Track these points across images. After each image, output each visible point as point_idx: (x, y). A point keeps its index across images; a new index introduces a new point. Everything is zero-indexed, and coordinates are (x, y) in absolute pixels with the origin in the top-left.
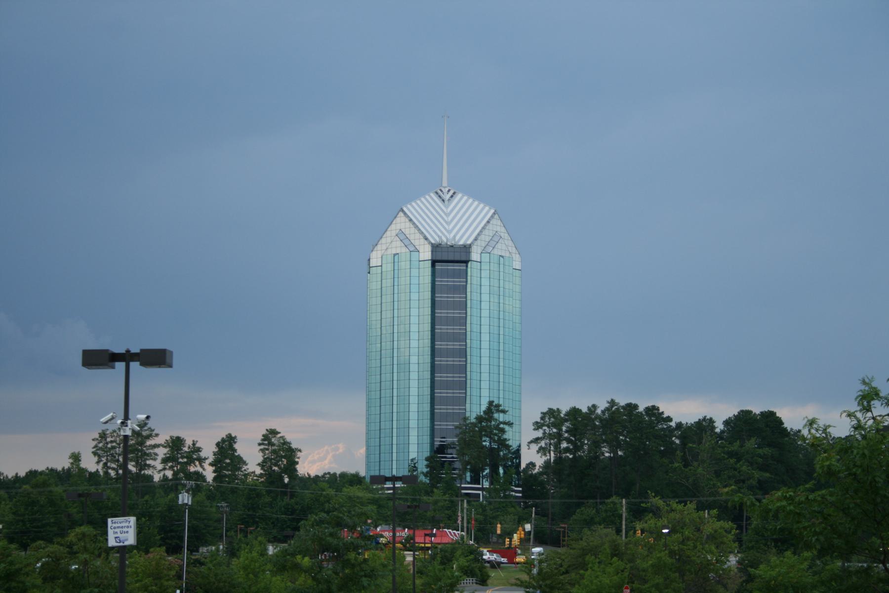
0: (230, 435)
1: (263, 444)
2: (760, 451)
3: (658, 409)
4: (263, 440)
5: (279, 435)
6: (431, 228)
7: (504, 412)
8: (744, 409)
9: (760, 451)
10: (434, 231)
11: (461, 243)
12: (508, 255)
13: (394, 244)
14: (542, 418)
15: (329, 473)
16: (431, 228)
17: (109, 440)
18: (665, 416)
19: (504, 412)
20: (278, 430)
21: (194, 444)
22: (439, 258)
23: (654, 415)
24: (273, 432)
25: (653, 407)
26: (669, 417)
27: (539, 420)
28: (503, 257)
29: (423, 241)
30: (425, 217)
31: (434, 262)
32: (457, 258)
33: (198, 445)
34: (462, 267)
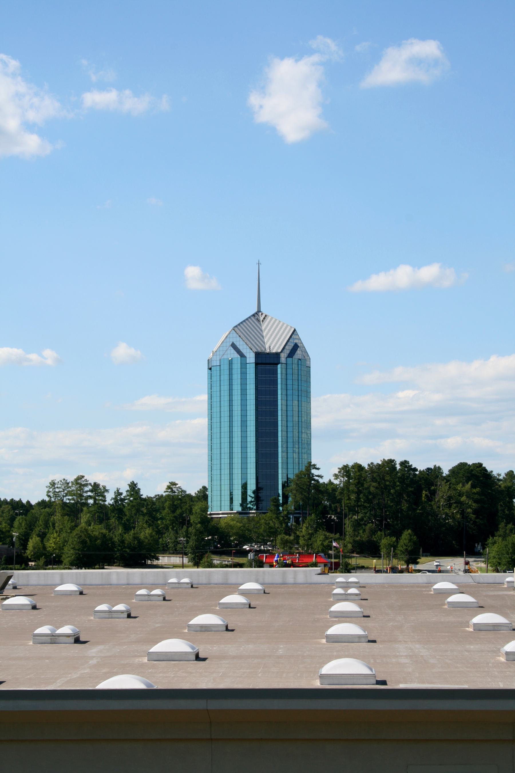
0: (133, 482)
1: (167, 492)
2: (474, 491)
3: (408, 462)
4: (167, 489)
5: (177, 486)
6: (254, 341)
7: (318, 469)
8: (462, 462)
9: (474, 491)
10: (255, 343)
11: (274, 351)
12: (303, 358)
13: (229, 352)
14: (339, 472)
15: (159, 495)
16: (254, 341)
17: (56, 486)
18: (413, 467)
19: (318, 469)
20: (177, 482)
21: (118, 491)
22: (260, 362)
23: (406, 467)
24: (174, 484)
25: (406, 461)
26: (415, 468)
27: (337, 473)
28: (300, 359)
29: (249, 350)
30: (278, 336)
31: (257, 364)
32: (267, 362)
33: (120, 491)
34: (271, 367)
